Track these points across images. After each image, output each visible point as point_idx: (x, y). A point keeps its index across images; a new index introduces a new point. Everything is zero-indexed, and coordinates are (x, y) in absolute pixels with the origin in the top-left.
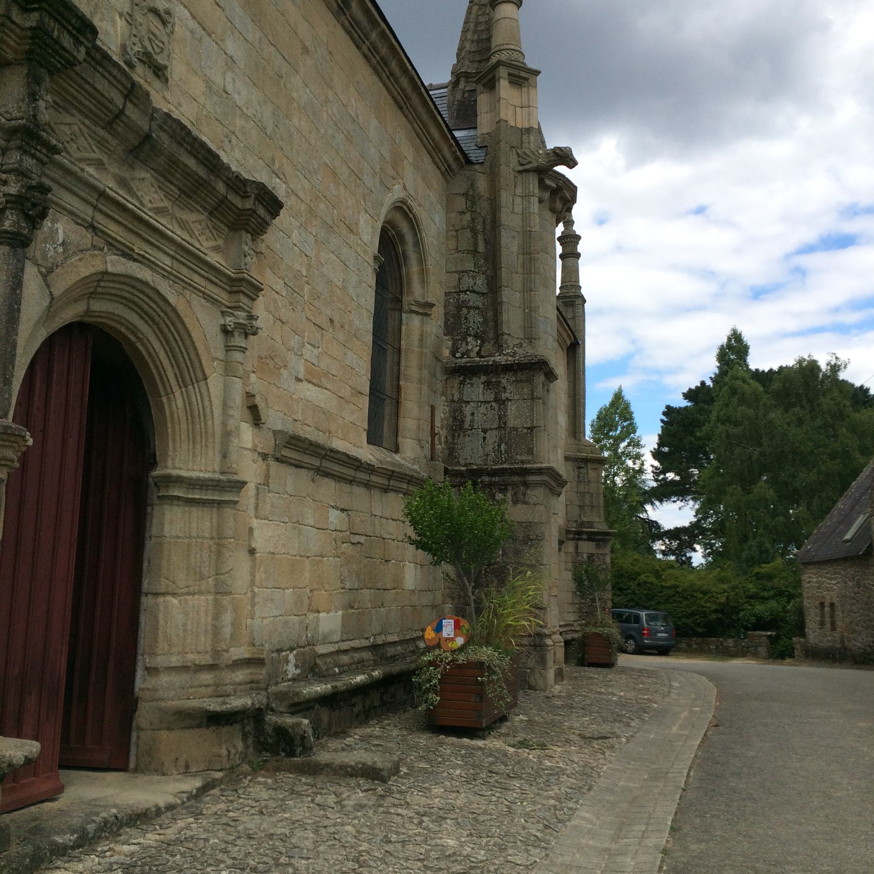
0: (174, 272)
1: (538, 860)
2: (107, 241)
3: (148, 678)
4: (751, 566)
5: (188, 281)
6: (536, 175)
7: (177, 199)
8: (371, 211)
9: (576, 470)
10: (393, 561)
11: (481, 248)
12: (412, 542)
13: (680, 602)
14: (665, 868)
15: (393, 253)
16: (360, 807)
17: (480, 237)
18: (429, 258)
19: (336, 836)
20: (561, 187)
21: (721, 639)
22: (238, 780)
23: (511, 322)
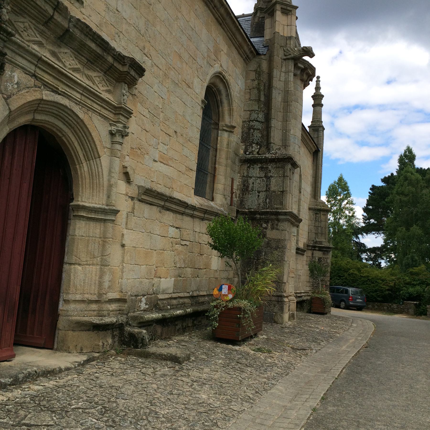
0: (82, 101)
1: (246, 409)
2: (43, 83)
3: (65, 305)
4: (408, 268)
5: (90, 106)
6: (293, 61)
7: (86, 64)
8: (201, 77)
9: (314, 215)
10: (205, 255)
11: (262, 99)
12: (211, 245)
13: (369, 284)
14: (311, 418)
15: (215, 100)
16: (164, 375)
17: (262, 93)
18: (234, 103)
19: (145, 389)
20: (307, 68)
21: (390, 304)
22: (107, 358)
23: (275, 137)
